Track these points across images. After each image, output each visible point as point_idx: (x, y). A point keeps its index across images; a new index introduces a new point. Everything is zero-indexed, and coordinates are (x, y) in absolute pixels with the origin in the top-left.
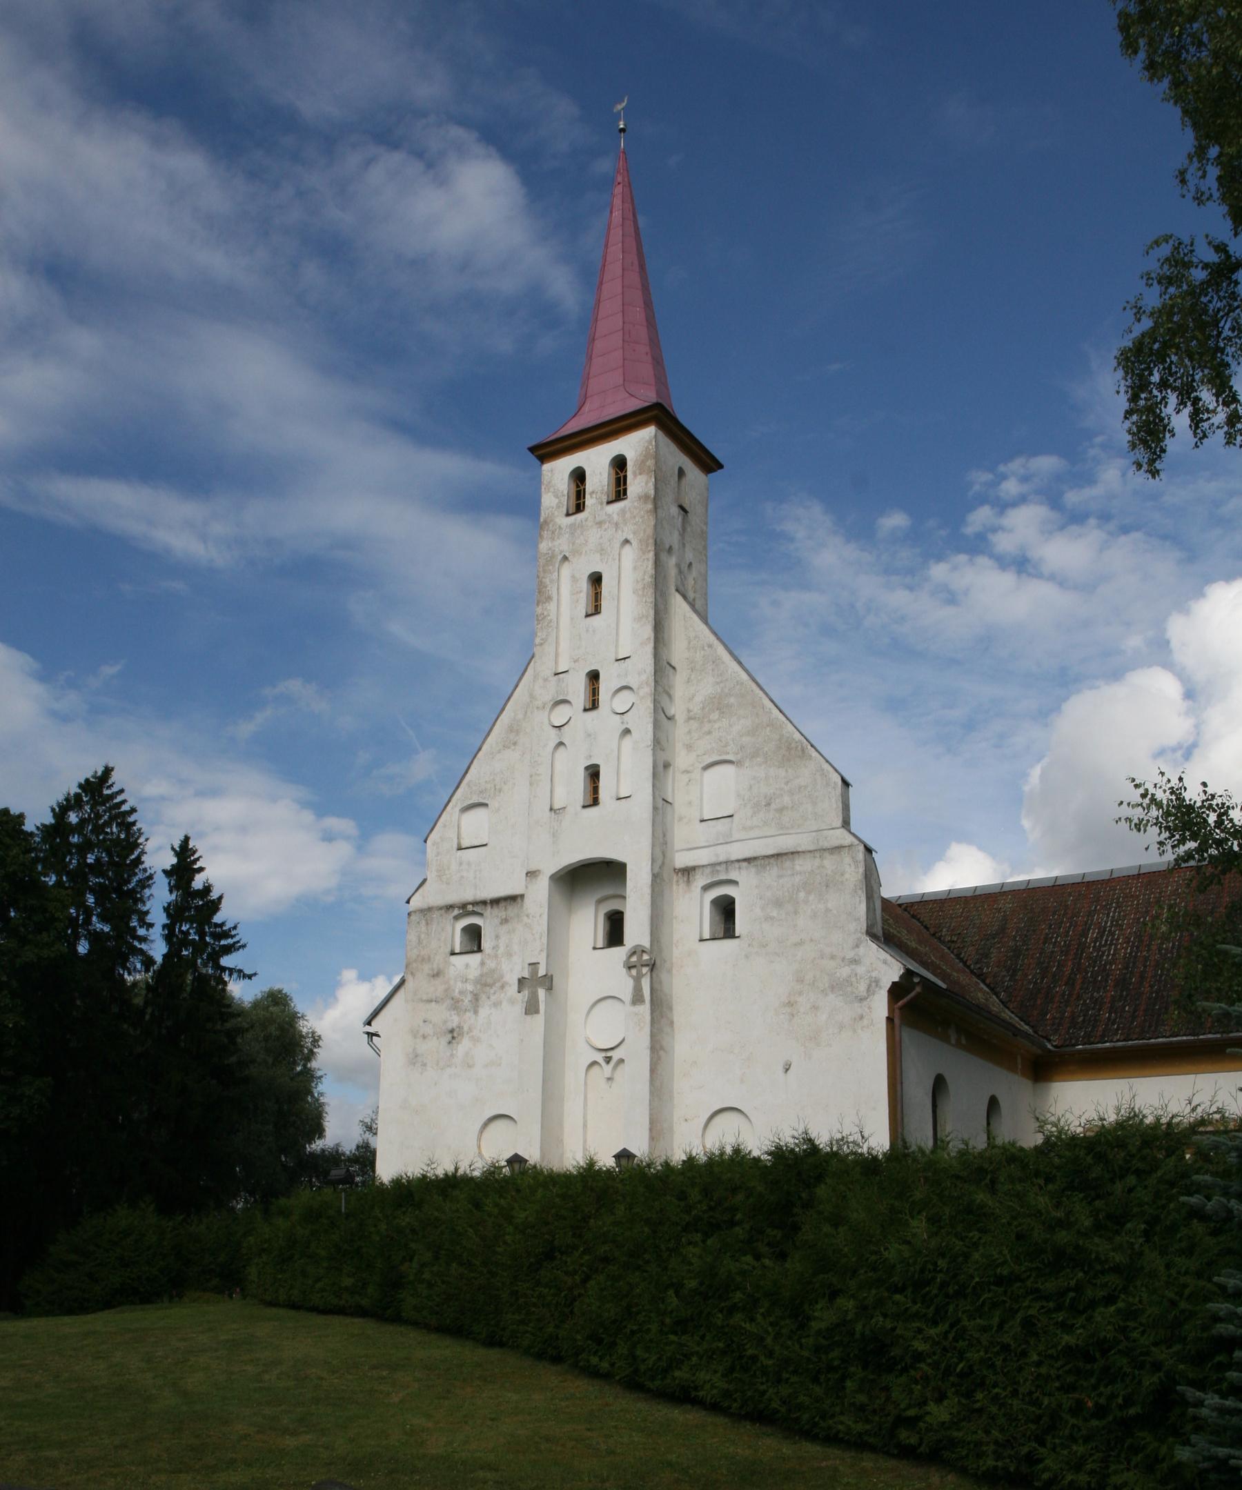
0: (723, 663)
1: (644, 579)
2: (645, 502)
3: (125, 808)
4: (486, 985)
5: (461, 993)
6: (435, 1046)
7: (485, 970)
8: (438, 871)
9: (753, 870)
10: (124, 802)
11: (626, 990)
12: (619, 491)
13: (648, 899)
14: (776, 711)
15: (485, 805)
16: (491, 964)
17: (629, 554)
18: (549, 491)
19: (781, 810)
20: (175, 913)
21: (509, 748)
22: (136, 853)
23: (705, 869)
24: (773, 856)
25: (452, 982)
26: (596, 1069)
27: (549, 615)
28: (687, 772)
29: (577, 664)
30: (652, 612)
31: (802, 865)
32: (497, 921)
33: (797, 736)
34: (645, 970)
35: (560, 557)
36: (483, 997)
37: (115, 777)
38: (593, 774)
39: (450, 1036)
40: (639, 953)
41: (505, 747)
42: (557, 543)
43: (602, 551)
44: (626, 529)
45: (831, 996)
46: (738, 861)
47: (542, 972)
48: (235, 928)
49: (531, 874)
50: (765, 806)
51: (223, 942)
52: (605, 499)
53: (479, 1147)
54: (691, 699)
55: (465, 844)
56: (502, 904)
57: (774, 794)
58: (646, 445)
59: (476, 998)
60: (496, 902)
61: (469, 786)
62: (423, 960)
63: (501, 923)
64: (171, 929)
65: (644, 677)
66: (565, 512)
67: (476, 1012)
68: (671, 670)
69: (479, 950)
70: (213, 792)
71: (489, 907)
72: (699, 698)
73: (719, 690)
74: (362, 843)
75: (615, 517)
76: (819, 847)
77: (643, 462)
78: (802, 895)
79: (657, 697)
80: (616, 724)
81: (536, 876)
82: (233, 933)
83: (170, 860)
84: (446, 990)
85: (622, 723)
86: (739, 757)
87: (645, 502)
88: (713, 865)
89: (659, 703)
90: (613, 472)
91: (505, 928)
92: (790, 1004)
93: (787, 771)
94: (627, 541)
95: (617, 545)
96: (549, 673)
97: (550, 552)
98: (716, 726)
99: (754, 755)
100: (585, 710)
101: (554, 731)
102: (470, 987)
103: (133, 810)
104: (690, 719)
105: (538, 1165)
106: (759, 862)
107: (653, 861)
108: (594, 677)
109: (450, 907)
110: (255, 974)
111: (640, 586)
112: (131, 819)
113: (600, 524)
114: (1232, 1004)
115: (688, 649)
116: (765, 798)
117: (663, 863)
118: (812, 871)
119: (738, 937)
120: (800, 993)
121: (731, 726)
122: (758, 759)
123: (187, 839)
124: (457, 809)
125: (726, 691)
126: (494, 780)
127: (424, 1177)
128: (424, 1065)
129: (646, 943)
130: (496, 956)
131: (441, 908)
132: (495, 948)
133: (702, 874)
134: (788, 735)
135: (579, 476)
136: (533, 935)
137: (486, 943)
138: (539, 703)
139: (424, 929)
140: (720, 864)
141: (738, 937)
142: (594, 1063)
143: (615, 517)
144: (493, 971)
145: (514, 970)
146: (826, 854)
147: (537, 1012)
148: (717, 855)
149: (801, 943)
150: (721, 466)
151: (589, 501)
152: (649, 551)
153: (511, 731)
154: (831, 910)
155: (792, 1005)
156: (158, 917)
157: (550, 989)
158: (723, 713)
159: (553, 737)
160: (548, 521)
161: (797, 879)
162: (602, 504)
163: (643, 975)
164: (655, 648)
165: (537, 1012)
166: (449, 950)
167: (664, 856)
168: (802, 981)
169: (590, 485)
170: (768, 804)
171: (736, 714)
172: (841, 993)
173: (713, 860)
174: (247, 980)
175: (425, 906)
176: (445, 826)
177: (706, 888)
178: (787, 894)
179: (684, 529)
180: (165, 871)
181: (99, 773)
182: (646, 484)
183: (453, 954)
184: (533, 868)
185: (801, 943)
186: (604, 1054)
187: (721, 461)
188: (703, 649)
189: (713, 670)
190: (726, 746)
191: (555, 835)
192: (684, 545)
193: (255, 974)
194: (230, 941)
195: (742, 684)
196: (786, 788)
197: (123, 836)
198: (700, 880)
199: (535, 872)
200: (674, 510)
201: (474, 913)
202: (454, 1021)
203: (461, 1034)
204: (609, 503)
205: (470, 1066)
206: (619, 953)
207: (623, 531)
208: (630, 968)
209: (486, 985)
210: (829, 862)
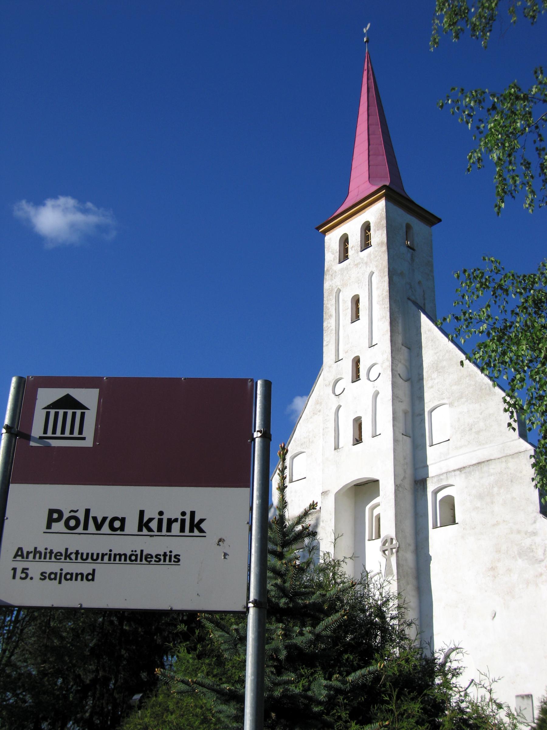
0: (438, 340)
1: (382, 294)
9: (463, 476)
12: (366, 243)
18: (329, 252)
19: (478, 433)
21: (316, 414)
23: (433, 478)
27: (331, 327)
29: (347, 354)
31: (494, 468)
42: (333, 282)
45: (520, 561)
46: (454, 471)
50: (469, 430)
52: (359, 249)
57: (474, 422)
58: (380, 212)
61: (295, 441)
69: (454, 522)
73: (436, 358)
74: (295, 534)
75: (365, 259)
76: (505, 455)
77: (379, 223)
78: (496, 489)
79: (394, 367)
81: (328, 494)
85: (374, 387)
92: (493, 569)
93: (480, 405)
97: (330, 288)
98: (436, 381)
99: (461, 397)
105: (255, 598)
106: (467, 470)
116: (468, 425)
118: (501, 472)
119: (457, 523)
120: (499, 560)
121: (444, 380)
122: (462, 400)
125: (441, 358)
126: (309, 436)
133: (432, 482)
134: (480, 381)
136: (326, 534)
140: (442, 474)
141: (457, 523)
143: (365, 259)
146: (510, 459)
149: (497, 524)
150: (440, 220)
151: (350, 253)
152: (385, 276)
153: (318, 404)
154: (515, 498)
155: (494, 569)
158: (440, 372)
160: (329, 269)
161: (492, 478)
162: (357, 253)
168: (500, 551)
171: (447, 372)
172: (526, 557)
178: (486, 490)
182: (382, 235)
185: (497, 524)
187: (439, 216)
189: (432, 346)
190: (442, 394)
195: (450, 351)
199: (326, 492)
207: (370, 267)
210: (512, 464)
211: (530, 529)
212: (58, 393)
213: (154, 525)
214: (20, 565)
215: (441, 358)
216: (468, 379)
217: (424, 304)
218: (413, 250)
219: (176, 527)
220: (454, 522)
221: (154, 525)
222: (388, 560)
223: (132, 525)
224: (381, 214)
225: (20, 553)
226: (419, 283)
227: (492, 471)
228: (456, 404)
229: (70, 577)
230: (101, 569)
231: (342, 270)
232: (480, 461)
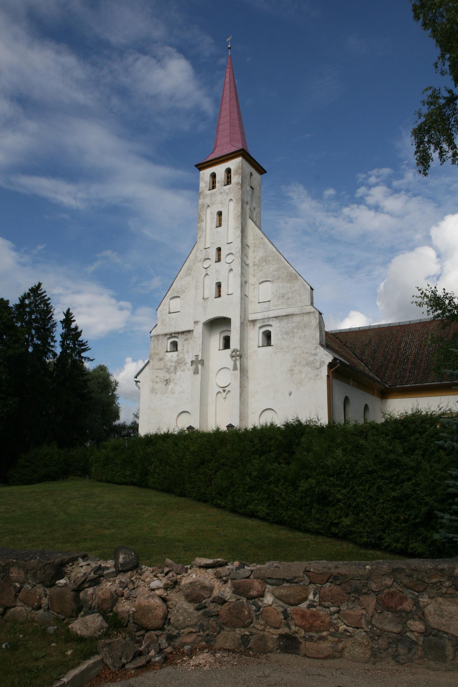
0: (267, 244)
1: (237, 214)
2: (238, 185)
3: (46, 298)
4: (179, 363)
5: (170, 366)
6: (160, 386)
7: (179, 358)
9: (278, 321)
10: (46, 296)
12: (228, 181)
14: (286, 262)
15: (179, 297)
16: (181, 356)
19: (288, 299)
20: (64, 337)
22: (50, 315)
24: (285, 316)
25: (167, 362)
26: (220, 394)
28: (253, 285)
30: (240, 226)
31: (296, 319)
32: (183, 340)
33: (294, 271)
34: (238, 358)
35: (206, 205)
36: (178, 368)
37: (42, 287)
38: (219, 285)
39: (166, 382)
42: (205, 200)
43: (222, 203)
44: (231, 195)
46: (272, 318)
47: (200, 359)
48: (87, 342)
49: (196, 322)
51: (82, 348)
52: (223, 184)
53: (177, 423)
54: (255, 258)
55: (171, 311)
56: (185, 334)
59: (176, 368)
60: (183, 333)
62: (156, 354)
63: (185, 341)
65: (237, 250)
66: (208, 189)
67: (175, 373)
69: (177, 350)
70: (79, 292)
71: (180, 335)
72: (258, 258)
73: (265, 255)
75: (227, 191)
77: (237, 170)
78: (296, 330)
80: (227, 267)
81: (198, 323)
82: (86, 344)
83: (63, 317)
84: (165, 365)
86: (272, 279)
88: (263, 319)
90: (226, 174)
91: (186, 342)
92: (291, 370)
93: (290, 284)
94: (231, 200)
96: (203, 248)
98: (264, 268)
99: (278, 279)
100: (216, 262)
101: (204, 270)
102: (173, 364)
103: (49, 299)
104: (254, 265)
107: (241, 317)
108: (219, 250)
109: (166, 335)
110: (94, 359)
111: (236, 216)
112: (48, 302)
114: (454, 370)
115: (254, 239)
117: (245, 318)
120: (295, 366)
121: (269, 268)
123: (69, 309)
124: (169, 299)
128: (157, 393)
129: (238, 348)
130: (183, 353)
131: (162, 335)
132: (183, 350)
135: (213, 176)
137: (179, 348)
138: (199, 259)
139: (156, 343)
140: (265, 319)
142: (219, 392)
143: (227, 191)
144: (182, 358)
145: (189, 358)
146: (305, 315)
147: (198, 373)
149: (295, 348)
150: (266, 172)
151: (217, 185)
153: (189, 270)
156: (58, 338)
157: (203, 365)
161: (294, 324)
162: (222, 186)
164: (242, 239)
165: (198, 373)
166: (165, 350)
169: (217, 179)
170: (283, 297)
173: (263, 317)
174: (91, 362)
175: (157, 334)
176: (164, 305)
177: (260, 328)
180: (61, 321)
181: (37, 285)
182: (238, 178)
183: (167, 352)
184: (196, 320)
185: (295, 348)
186: (223, 389)
187: (266, 170)
190: (268, 275)
191: (205, 308)
192: (252, 201)
193: (94, 359)
194: (85, 347)
196: (290, 291)
197: (45, 308)
198: (258, 325)
199: (197, 322)
200: (249, 188)
201: (175, 337)
202: (168, 376)
203: (170, 381)
204: (224, 185)
206: (228, 352)
210: (306, 318)
211: (314, 352)
215: (268, 255)
216: (283, 269)
220: (177, 350)
222: (235, 362)
224: (239, 165)
227: (294, 320)
228: (275, 282)
232: (288, 314)
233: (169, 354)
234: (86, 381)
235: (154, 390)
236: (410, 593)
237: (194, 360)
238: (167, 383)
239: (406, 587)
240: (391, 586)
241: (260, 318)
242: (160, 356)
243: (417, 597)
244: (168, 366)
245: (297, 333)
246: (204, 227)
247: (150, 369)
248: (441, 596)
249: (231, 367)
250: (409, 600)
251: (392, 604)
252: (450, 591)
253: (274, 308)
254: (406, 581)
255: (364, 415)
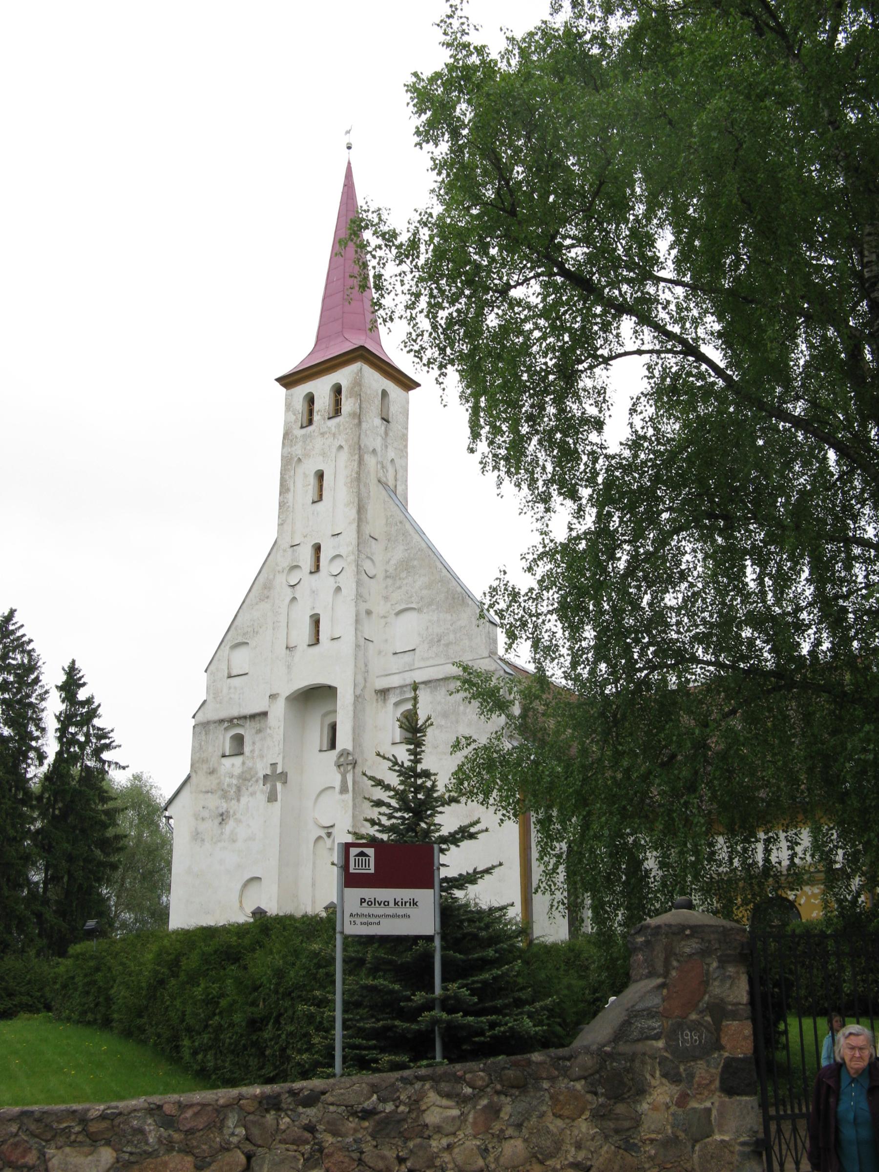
2: (354, 418)
3: (24, 639)
4: (245, 780)
5: (229, 785)
6: (210, 826)
7: (245, 769)
8: (214, 694)
9: (428, 690)
10: (24, 635)
11: (337, 783)
13: (351, 714)
14: (444, 570)
15: (247, 643)
16: (249, 764)
17: (344, 456)
19: (447, 645)
20: (66, 720)
22: (36, 674)
24: (442, 679)
25: (222, 778)
26: (321, 842)
28: (385, 617)
30: (356, 499)
32: (254, 731)
33: (459, 589)
34: (350, 767)
35: (296, 459)
36: (244, 788)
37: (17, 618)
38: (316, 622)
39: (220, 818)
40: (345, 755)
41: (261, 600)
42: (293, 449)
43: (324, 454)
44: (340, 438)
47: (279, 770)
48: (112, 731)
49: (273, 697)
51: (103, 742)
53: (241, 902)
54: (388, 562)
55: (234, 673)
56: (257, 719)
59: (239, 789)
60: (253, 717)
62: (203, 761)
63: (257, 733)
64: (62, 731)
65: (351, 548)
67: (238, 800)
68: (374, 541)
69: (241, 753)
71: (248, 721)
72: (393, 562)
80: (331, 583)
82: (110, 735)
83: (62, 678)
84: (219, 784)
86: (420, 605)
87: (354, 418)
88: (401, 687)
89: (362, 566)
90: (332, 395)
91: (260, 736)
94: (341, 447)
95: (334, 450)
96: (287, 545)
98: (405, 582)
99: (430, 604)
100: (311, 573)
101: (289, 590)
102: (235, 781)
103: (31, 641)
104: (387, 577)
106: (432, 684)
107: (355, 685)
108: (317, 548)
109: (222, 721)
110: (128, 766)
111: (349, 480)
112: (29, 648)
113: (323, 434)
115: (387, 524)
117: (365, 687)
123: (73, 662)
124: (228, 647)
125: (412, 555)
127: (277, 915)
128: (203, 840)
129: (350, 748)
130: (253, 758)
131: (215, 722)
132: (252, 751)
135: (310, 400)
137: (247, 749)
138: (280, 568)
139: (204, 738)
142: (320, 838)
144: (251, 769)
145: (263, 769)
147: (276, 800)
148: (404, 680)
150: (418, 385)
151: (316, 418)
156: (51, 724)
157: (285, 782)
159: (288, 593)
163: (348, 771)
164: (359, 526)
165: (276, 800)
166: (220, 754)
167: (365, 681)
169: (317, 407)
170: (439, 641)
173: (402, 683)
174: (122, 770)
175: (205, 720)
176: (219, 660)
177: (397, 704)
179: (386, 434)
180: (57, 687)
181: (6, 614)
183: (224, 756)
184: (274, 692)
186: (326, 831)
188: (396, 524)
191: (289, 667)
192: (386, 447)
193: (128, 766)
194: (107, 741)
196: (452, 628)
197: (26, 661)
198: (393, 699)
200: (378, 421)
201: (238, 725)
202: (224, 806)
203: (228, 817)
204: (329, 418)
205: (234, 841)
206: (334, 754)
208: (339, 766)
209: (245, 780)
212: (358, 850)
213: (400, 904)
214: (352, 919)
215: (412, 555)
217: (396, 486)
218: (388, 421)
219: (408, 904)
221: (400, 904)
223: (392, 904)
225: (351, 915)
226: (392, 461)
229: (371, 924)
230: (382, 920)
231: (304, 436)
233: (227, 762)
234: (111, 814)
235: (198, 834)
236: (36, 1143)
237: (269, 773)
238: (223, 820)
239: (33, 1135)
240: (16, 1135)
241: (396, 685)
242: (211, 766)
243: (44, 1147)
244: (225, 786)
245: (465, 713)
246: (290, 504)
247: (191, 793)
248: (69, 1146)
249: (337, 784)
250: (34, 1152)
251: (13, 1158)
252: (80, 1138)
253: (422, 664)
254: (33, 1127)
255: (241, 902)
